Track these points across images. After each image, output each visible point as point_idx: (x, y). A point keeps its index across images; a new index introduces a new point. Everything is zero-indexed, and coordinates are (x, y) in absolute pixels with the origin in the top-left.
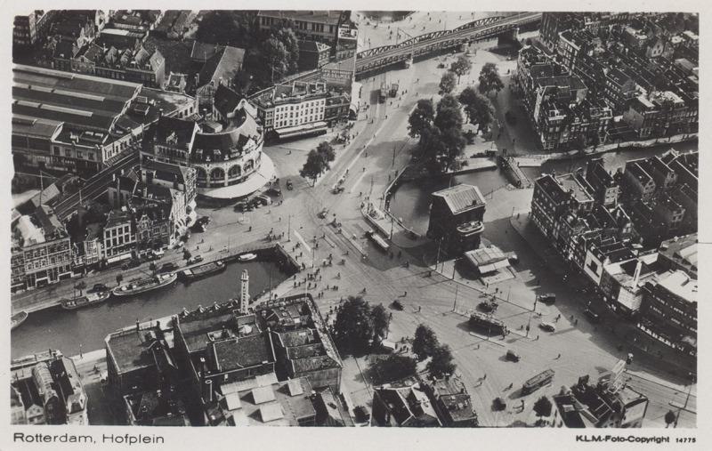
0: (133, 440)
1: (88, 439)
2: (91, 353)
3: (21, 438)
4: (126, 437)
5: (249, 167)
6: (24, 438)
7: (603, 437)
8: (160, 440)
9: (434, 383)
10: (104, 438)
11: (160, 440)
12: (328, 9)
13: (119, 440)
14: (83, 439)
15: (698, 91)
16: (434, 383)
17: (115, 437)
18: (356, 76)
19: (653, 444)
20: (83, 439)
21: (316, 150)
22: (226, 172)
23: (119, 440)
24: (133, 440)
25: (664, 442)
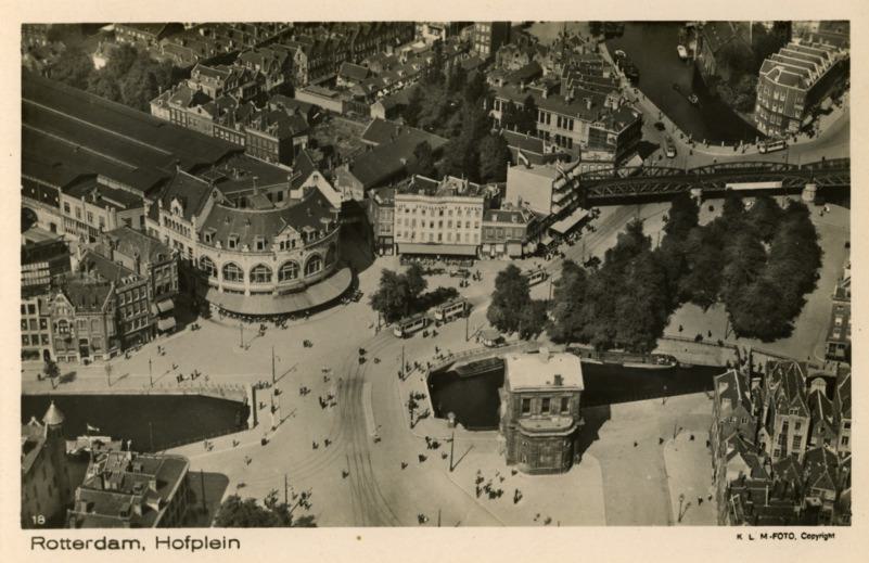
0: (197, 544)
1: (135, 544)
2: (652, 104)
3: (41, 544)
4: (187, 540)
5: (288, 274)
6: (45, 545)
7: (770, 534)
8: (234, 544)
9: (694, 146)
10: (158, 542)
11: (234, 544)
12: (852, 304)
13: (178, 544)
14: (127, 545)
15: (509, 23)
16: (694, 146)
17: (171, 541)
18: (143, 110)
19: (821, 540)
20: (127, 545)
21: (770, 26)
22: (275, 271)
23: (178, 544)
24: (197, 544)
25: (830, 539)
